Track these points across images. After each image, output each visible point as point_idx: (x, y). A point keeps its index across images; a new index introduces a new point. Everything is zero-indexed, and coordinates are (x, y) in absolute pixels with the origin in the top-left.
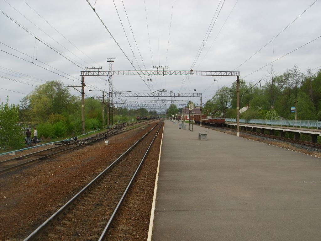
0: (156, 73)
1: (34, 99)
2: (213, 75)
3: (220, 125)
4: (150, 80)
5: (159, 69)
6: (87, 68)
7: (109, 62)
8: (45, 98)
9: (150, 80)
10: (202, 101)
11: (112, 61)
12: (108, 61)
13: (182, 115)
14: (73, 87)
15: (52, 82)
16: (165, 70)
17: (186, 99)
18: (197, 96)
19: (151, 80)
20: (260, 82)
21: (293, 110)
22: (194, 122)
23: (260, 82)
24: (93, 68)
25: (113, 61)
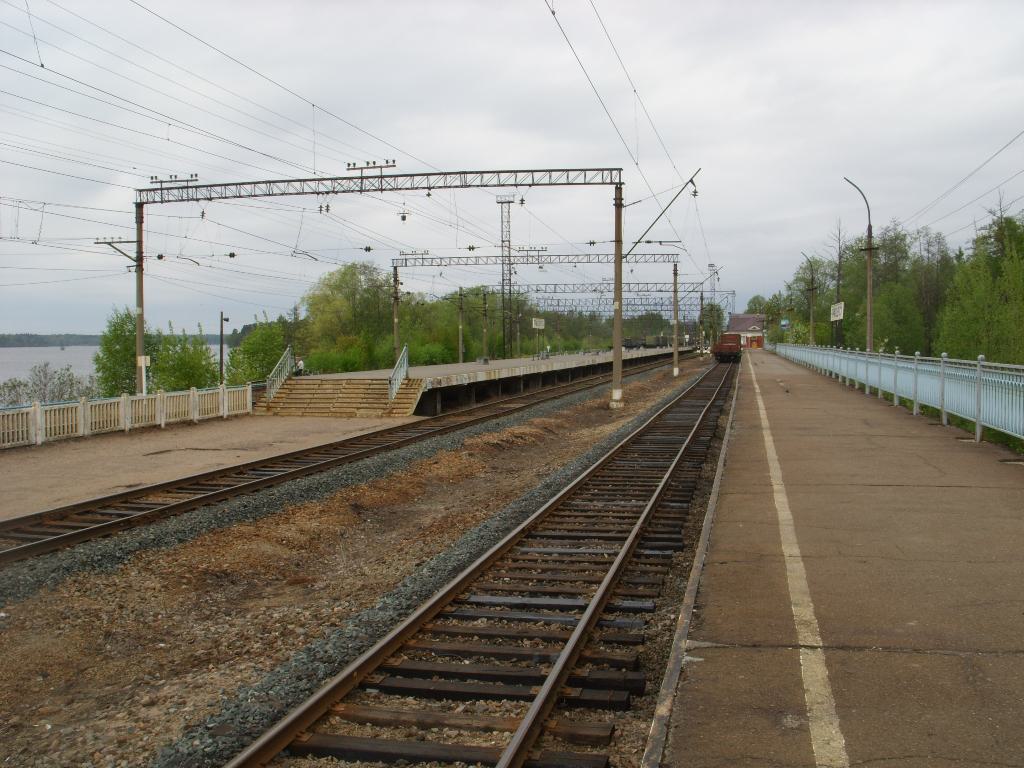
1: (316, 303)
5: (367, 173)
7: (502, 203)
8: (340, 301)
14: (109, 244)
15: (354, 266)
16: (386, 172)
20: (691, 181)
21: (784, 326)
23: (691, 181)
24: (173, 178)
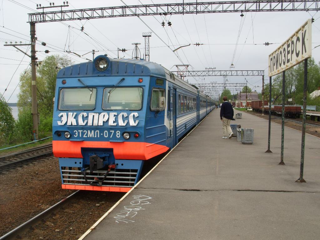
0: (181, 8)
2: (308, 10)
3: (294, 115)
4: (166, 24)
6: (39, 7)
7: (145, 36)
9: (166, 24)
10: (264, 81)
11: (149, 36)
12: (143, 36)
13: (237, 102)
17: (241, 80)
18: (257, 74)
19: (170, 24)
22: (252, 110)
24: (52, 5)
25: (150, 36)
